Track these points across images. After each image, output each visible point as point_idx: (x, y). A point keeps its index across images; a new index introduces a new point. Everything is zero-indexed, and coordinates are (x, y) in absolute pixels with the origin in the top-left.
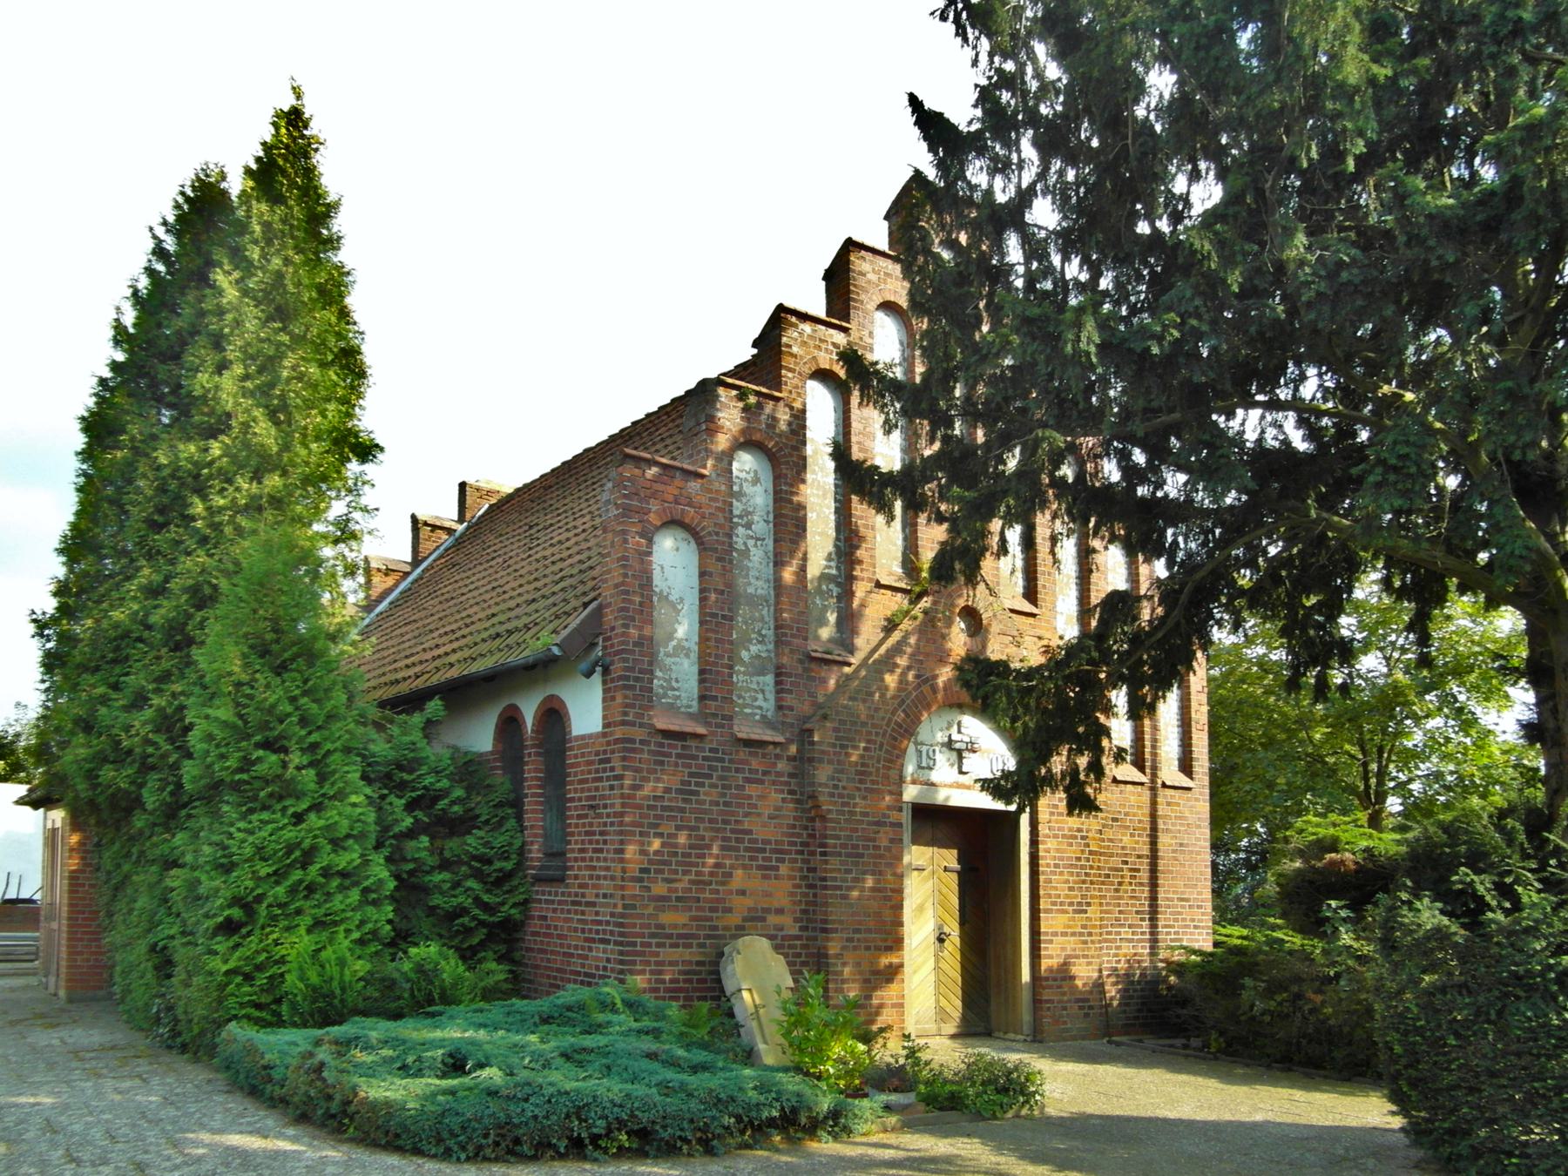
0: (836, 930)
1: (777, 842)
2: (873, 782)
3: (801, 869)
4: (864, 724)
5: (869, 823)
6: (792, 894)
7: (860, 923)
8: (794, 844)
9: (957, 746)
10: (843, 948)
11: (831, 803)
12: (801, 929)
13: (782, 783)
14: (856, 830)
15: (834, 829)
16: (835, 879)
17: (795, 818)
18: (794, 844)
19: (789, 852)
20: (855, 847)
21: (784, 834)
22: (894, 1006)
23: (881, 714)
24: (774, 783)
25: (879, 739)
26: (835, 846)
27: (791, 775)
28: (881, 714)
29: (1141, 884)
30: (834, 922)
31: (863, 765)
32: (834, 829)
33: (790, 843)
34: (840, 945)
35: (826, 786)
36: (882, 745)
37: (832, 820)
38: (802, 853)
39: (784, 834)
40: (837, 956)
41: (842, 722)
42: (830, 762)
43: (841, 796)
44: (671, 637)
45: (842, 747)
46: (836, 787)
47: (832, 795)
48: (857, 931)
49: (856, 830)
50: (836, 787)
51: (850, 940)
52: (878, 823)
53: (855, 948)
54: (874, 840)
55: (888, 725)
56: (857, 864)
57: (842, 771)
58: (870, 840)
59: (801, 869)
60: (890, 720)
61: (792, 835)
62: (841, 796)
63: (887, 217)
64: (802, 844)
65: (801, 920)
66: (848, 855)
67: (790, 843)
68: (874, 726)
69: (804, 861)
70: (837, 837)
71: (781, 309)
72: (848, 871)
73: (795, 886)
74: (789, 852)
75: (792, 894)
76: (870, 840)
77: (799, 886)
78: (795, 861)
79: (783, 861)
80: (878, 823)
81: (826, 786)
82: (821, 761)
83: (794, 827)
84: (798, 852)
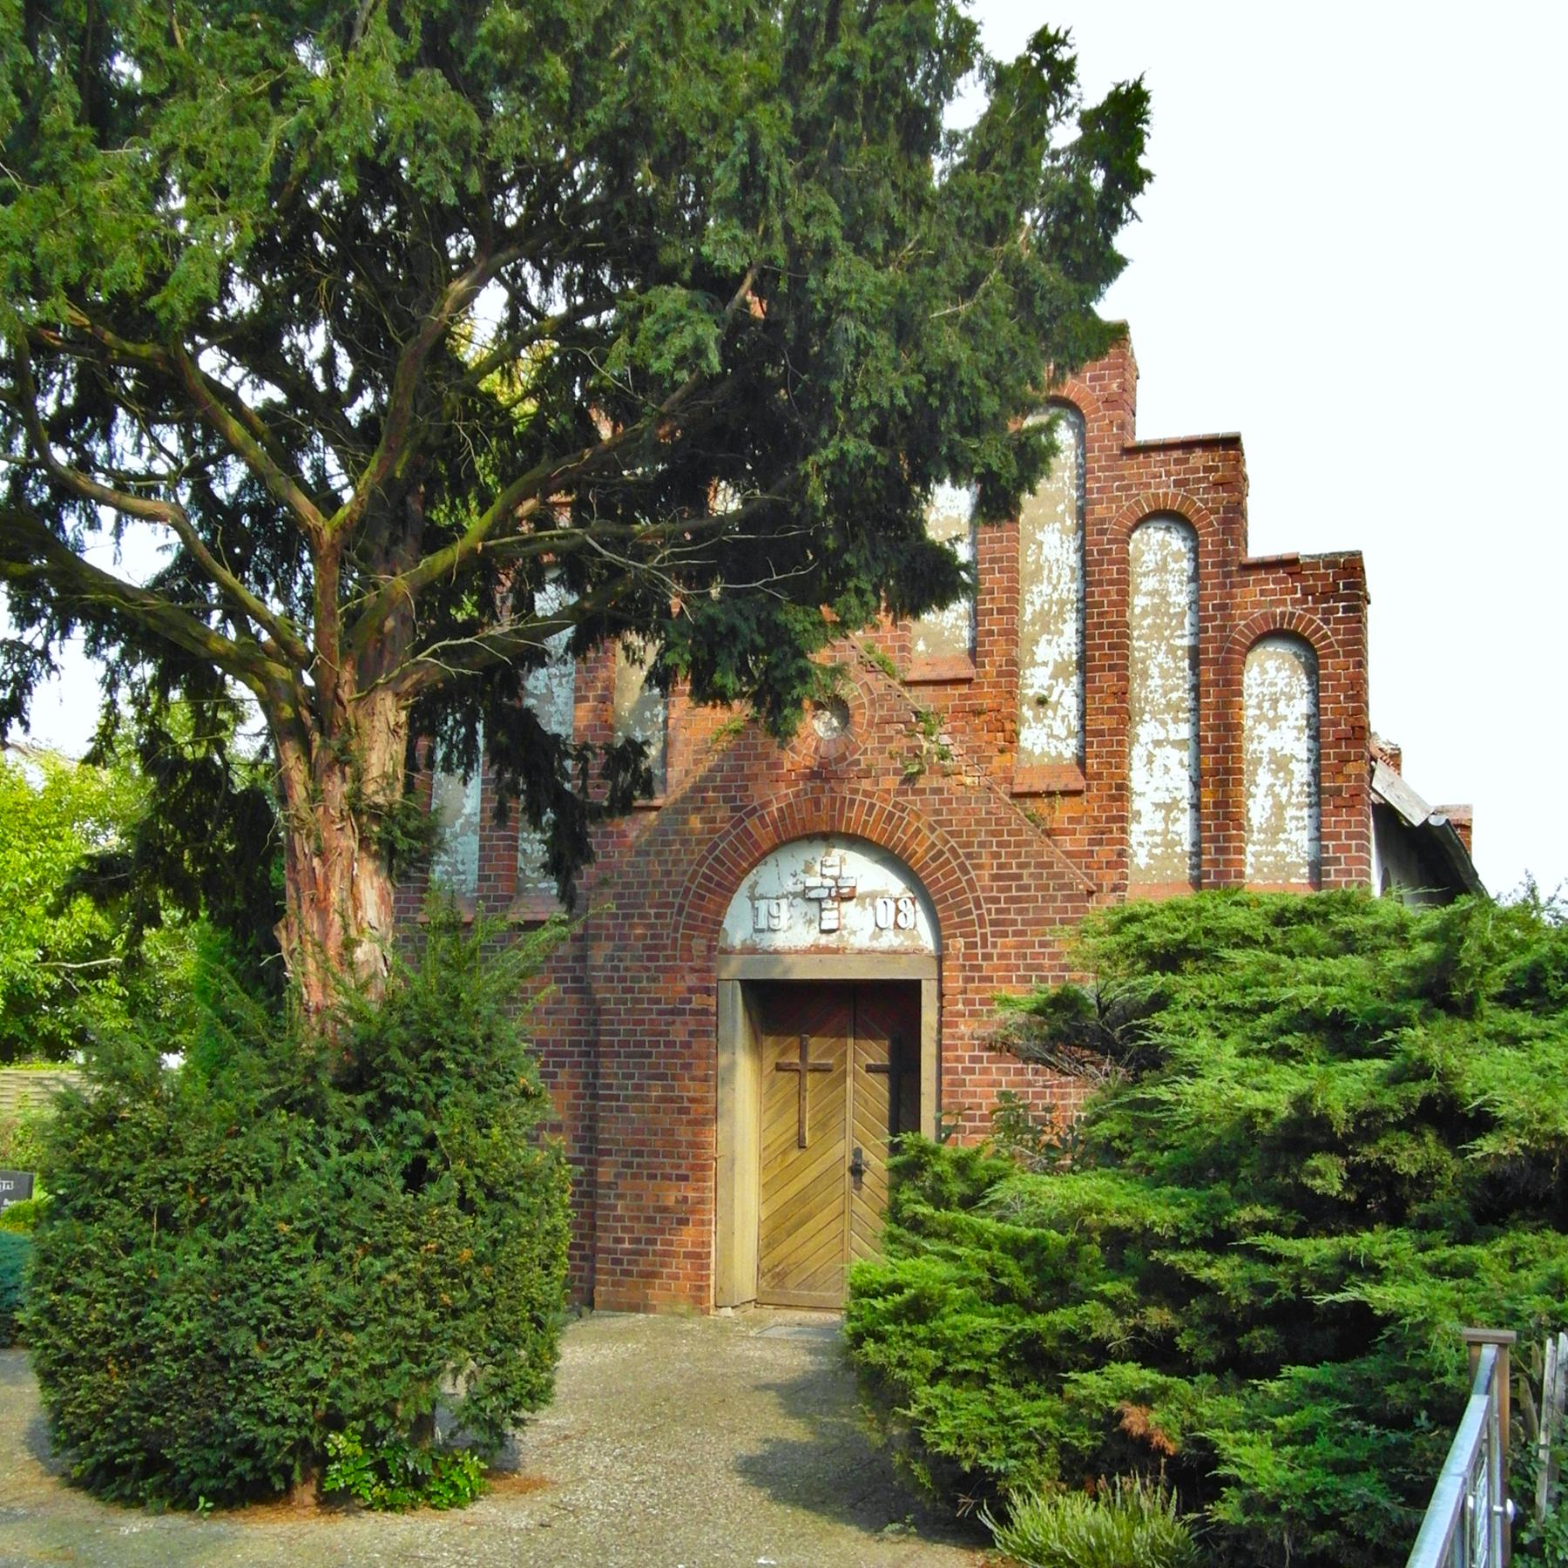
0: (609, 1152)
1: (556, 1043)
2: (667, 958)
3: (585, 1075)
4: (657, 884)
5: (660, 1013)
6: (570, 1107)
7: (642, 1143)
8: (578, 1044)
9: (813, 894)
10: (617, 1175)
11: (608, 990)
12: (582, 1150)
13: (567, 969)
14: (642, 1022)
15: (611, 1022)
16: (610, 1087)
17: (580, 1012)
18: (578, 1044)
19: (571, 1054)
20: (641, 1044)
21: (563, 1032)
22: (687, 1255)
23: (683, 867)
24: (554, 970)
25: (677, 901)
26: (611, 1044)
27: (575, 959)
28: (683, 867)
29: (607, 1251)
30: (606, 1141)
31: (654, 937)
32: (611, 1022)
33: (572, 1043)
34: (613, 1171)
35: (602, 968)
36: (681, 907)
37: (608, 1012)
38: (587, 1054)
39: (563, 1032)
40: (609, 1186)
41: (627, 885)
42: (610, 938)
43: (622, 980)
44: (458, 814)
45: (626, 917)
46: (616, 969)
47: (611, 980)
48: (639, 1154)
49: (642, 1022)
50: (616, 969)
51: (628, 1165)
52: (672, 1012)
53: (634, 1176)
54: (667, 1033)
55: (692, 880)
56: (641, 1066)
57: (624, 949)
58: (661, 1034)
59: (585, 1075)
60: (695, 873)
61: (574, 1033)
62: (622, 980)
63: (1119, 263)
64: (587, 1044)
65: (583, 1139)
66: (629, 1055)
67: (572, 1043)
68: (671, 884)
69: (589, 1065)
70: (615, 1033)
71: (1231, 443)
72: (630, 1076)
73: (576, 1097)
74: (571, 1054)
75: (570, 1107)
76: (661, 1034)
77: (582, 1097)
78: (579, 1064)
79: (562, 1065)
80: (672, 1012)
81: (602, 968)
82: (597, 938)
83: (579, 1022)
84: (581, 1054)
